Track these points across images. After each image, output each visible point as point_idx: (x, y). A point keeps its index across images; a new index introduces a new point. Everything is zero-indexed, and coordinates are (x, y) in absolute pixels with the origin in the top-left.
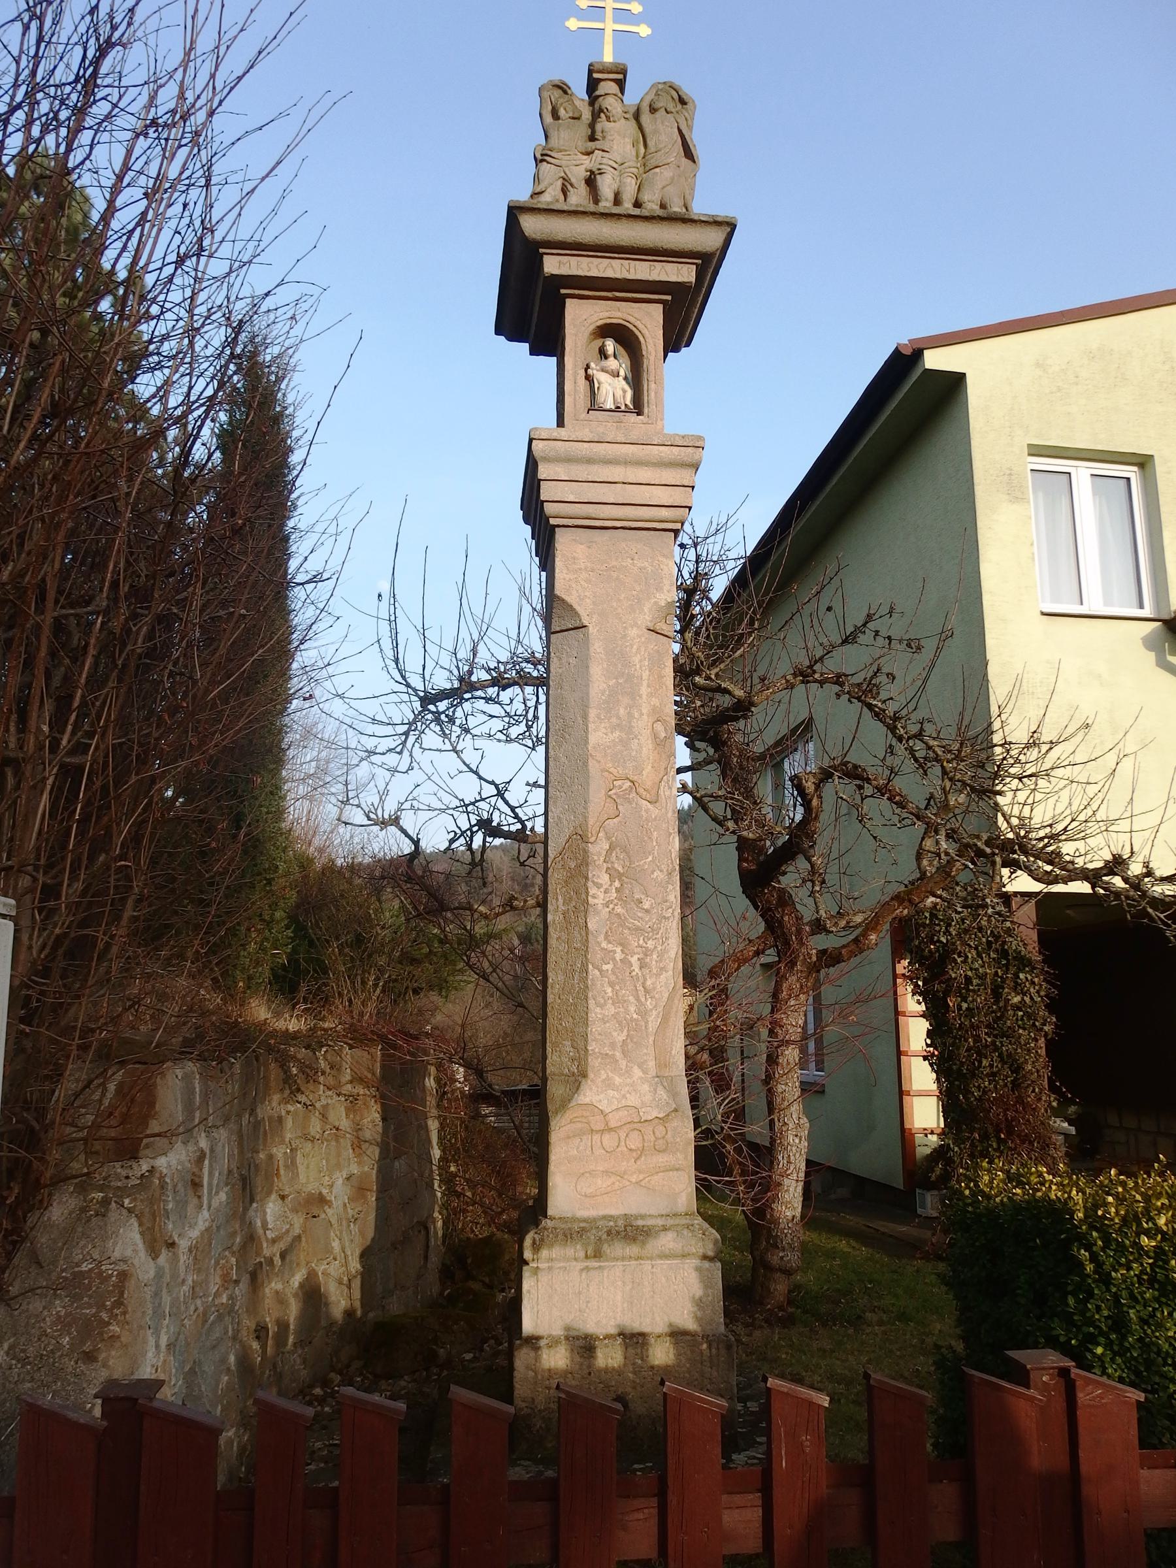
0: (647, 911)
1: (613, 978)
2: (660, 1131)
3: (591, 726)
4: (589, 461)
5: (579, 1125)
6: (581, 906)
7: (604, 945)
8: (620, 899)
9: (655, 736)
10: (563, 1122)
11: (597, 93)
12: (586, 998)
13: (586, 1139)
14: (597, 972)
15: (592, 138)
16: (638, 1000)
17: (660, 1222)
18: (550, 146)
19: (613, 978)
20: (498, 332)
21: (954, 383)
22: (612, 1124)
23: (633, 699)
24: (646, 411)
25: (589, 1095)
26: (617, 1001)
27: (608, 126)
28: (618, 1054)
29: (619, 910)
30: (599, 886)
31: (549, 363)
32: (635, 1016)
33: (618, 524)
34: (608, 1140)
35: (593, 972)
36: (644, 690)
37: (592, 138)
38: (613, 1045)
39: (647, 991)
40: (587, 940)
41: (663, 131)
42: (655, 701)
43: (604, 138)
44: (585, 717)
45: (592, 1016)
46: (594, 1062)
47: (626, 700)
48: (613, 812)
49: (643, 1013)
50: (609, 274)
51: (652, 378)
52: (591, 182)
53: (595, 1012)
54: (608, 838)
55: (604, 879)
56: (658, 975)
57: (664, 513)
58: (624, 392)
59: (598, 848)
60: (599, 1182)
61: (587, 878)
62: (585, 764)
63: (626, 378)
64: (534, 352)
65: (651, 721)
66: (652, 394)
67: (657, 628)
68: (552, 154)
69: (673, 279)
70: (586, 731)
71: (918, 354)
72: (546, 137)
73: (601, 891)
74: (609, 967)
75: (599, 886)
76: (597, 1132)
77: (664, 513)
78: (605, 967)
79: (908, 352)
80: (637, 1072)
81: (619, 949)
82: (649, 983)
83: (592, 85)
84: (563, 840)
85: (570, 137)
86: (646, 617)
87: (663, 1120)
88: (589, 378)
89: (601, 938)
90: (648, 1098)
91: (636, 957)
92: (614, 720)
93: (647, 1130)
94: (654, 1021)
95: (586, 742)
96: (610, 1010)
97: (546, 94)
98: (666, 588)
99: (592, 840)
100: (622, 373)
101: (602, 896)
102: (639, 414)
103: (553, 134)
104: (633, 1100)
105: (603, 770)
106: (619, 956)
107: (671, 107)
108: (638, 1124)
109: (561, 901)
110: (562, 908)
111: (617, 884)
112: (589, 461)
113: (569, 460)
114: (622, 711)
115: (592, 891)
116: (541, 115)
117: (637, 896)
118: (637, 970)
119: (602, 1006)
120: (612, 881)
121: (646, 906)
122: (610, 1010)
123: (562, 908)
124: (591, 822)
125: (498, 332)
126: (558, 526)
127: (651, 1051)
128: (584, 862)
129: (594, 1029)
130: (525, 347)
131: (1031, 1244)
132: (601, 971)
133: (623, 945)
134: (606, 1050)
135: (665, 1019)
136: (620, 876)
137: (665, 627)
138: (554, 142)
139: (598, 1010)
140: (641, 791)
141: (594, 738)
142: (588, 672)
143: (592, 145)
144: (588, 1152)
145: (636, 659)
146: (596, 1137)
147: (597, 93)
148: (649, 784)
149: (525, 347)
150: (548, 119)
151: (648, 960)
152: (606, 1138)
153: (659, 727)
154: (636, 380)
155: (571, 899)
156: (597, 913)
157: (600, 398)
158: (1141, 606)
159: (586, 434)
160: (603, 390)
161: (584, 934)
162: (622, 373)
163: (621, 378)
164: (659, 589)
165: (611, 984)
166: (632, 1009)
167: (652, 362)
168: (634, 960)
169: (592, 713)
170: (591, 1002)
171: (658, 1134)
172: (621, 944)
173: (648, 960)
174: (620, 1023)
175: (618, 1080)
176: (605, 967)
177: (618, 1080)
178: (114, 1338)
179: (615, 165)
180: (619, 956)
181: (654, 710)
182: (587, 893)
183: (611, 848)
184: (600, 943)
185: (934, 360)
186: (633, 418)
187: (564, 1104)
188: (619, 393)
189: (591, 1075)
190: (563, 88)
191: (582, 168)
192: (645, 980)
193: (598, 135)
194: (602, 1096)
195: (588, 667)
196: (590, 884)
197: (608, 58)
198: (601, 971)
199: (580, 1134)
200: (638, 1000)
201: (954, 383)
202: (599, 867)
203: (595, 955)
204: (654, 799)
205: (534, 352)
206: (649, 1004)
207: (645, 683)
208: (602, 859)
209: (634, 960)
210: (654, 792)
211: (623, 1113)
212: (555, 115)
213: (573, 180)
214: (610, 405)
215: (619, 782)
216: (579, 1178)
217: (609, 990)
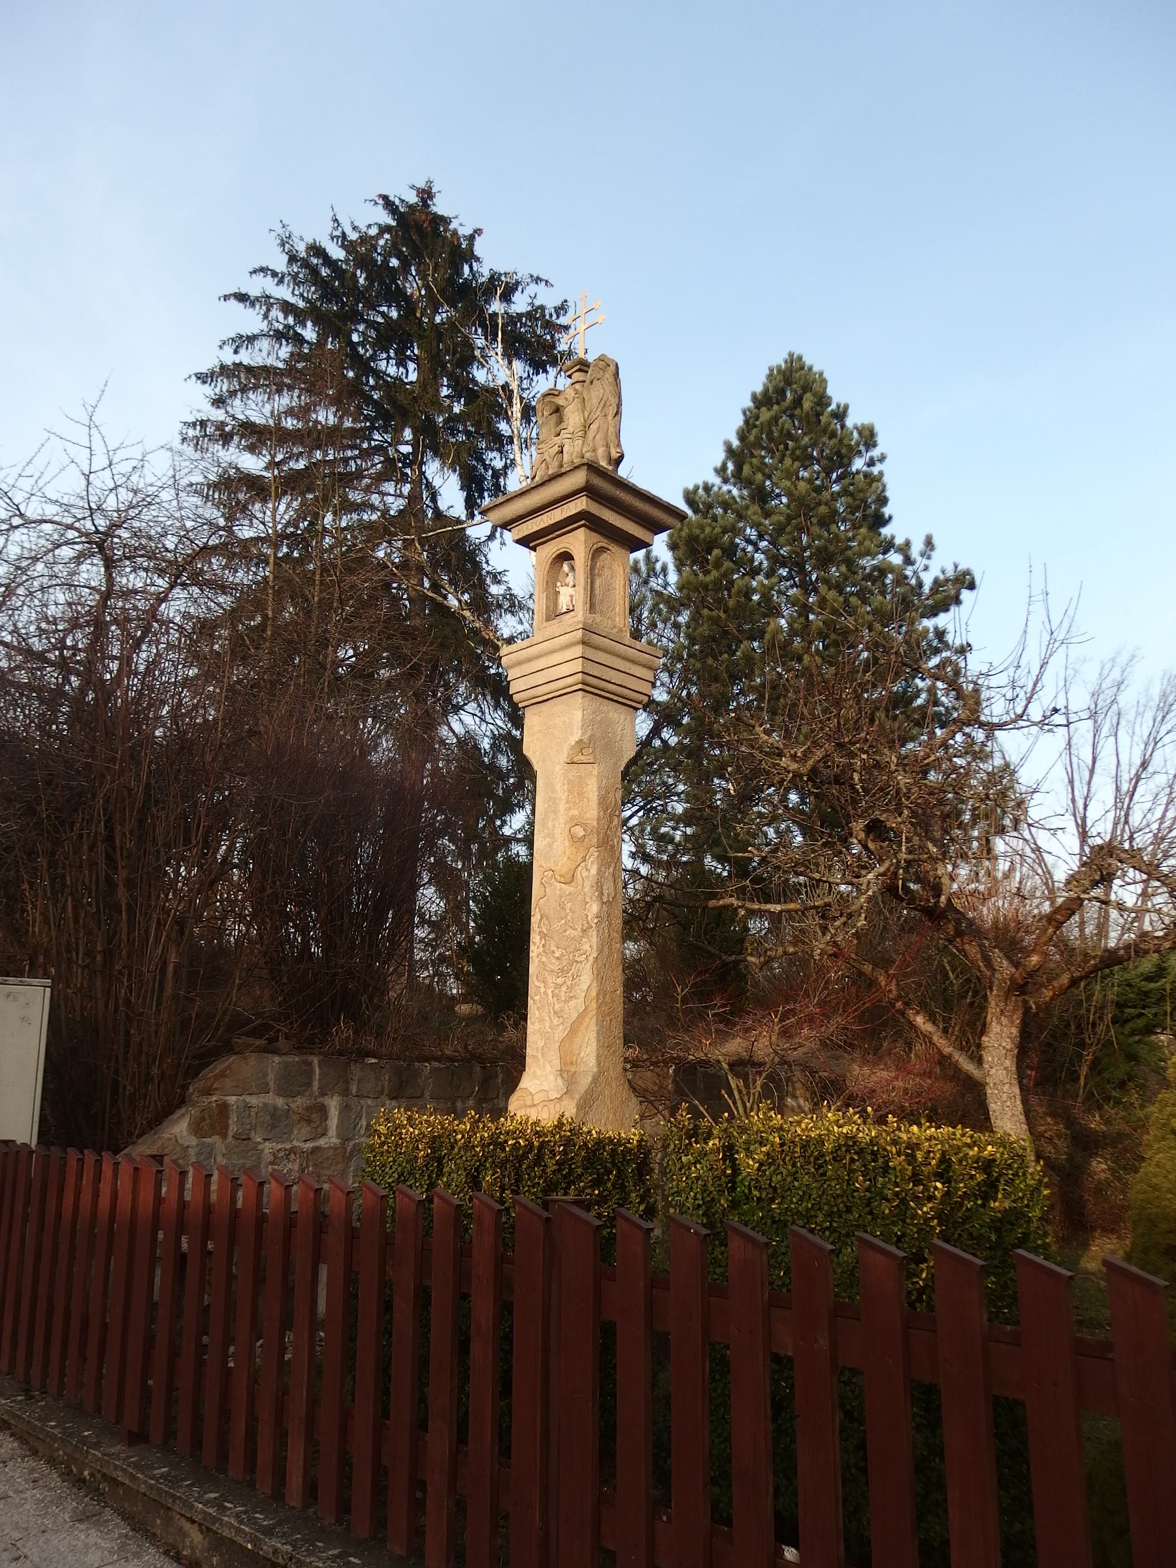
4: (529, 660)
29: (544, 959)
33: (550, 696)
47: (552, 816)
50: (542, 526)
57: (570, 680)
60: (1133, 936)
65: (568, 827)
67: (575, 760)
69: (574, 512)
77: (570, 680)
80: (548, 1068)
86: (564, 757)
87: (560, 1099)
90: (552, 1085)
93: (551, 1105)
104: (546, 1087)
112: (529, 660)
113: (519, 663)
137: (583, 758)
159: (547, 635)
164: (572, 734)
165: (538, 1009)
168: (549, 992)
178: (599, 1133)
209: (549, 992)
211: (541, 1095)
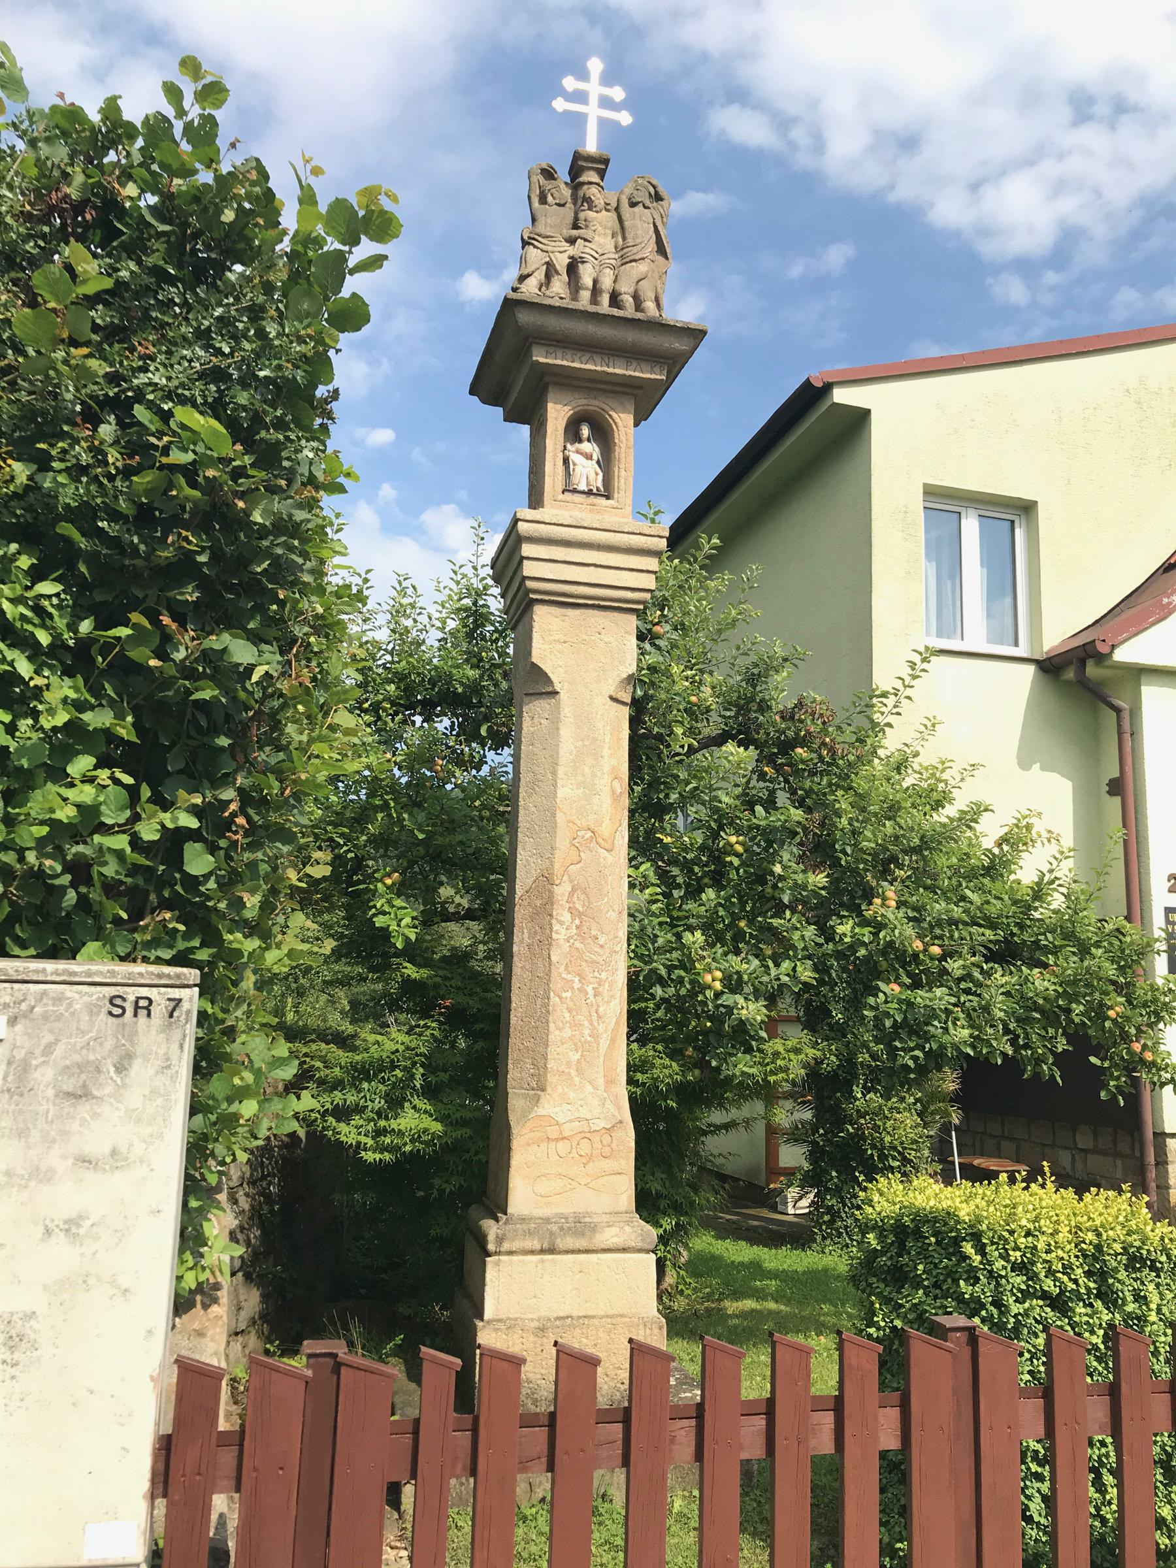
0: (602, 946)
1: (571, 1004)
2: (606, 1139)
3: (560, 783)
5: (539, 1134)
6: (545, 941)
7: (564, 976)
8: (579, 935)
9: (613, 791)
10: (524, 1131)
11: (581, 179)
12: (547, 1022)
13: (544, 1145)
14: (557, 999)
15: (576, 226)
16: (592, 1024)
17: (605, 1218)
18: (537, 231)
19: (571, 1004)
20: (472, 392)
21: (860, 418)
22: (566, 1134)
23: (596, 759)
24: (616, 495)
25: (548, 1107)
26: (575, 1025)
27: (591, 214)
28: (573, 1073)
29: (578, 945)
30: (561, 923)
31: (524, 431)
32: (589, 1039)
34: (562, 1147)
35: (554, 1000)
36: (606, 752)
37: (576, 226)
38: (569, 1064)
39: (599, 1017)
40: (550, 970)
41: (640, 223)
42: (614, 762)
43: (587, 226)
44: (554, 773)
45: (551, 1037)
46: (551, 1079)
48: (576, 859)
49: (595, 1036)
51: (622, 466)
52: (573, 268)
53: (555, 1035)
54: (571, 881)
55: (566, 917)
56: (608, 1002)
58: (597, 474)
59: (562, 890)
61: (551, 915)
62: (554, 815)
63: (598, 462)
64: (508, 418)
66: (622, 481)
68: (540, 239)
70: (555, 786)
71: (828, 388)
72: (534, 220)
73: (563, 927)
74: (568, 994)
75: (561, 923)
76: (553, 1140)
78: (564, 995)
79: (819, 384)
80: (589, 1088)
81: (576, 979)
82: (601, 1009)
83: (575, 171)
84: (530, 881)
85: (555, 219)
88: (566, 461)
89: (562, 969)
91: (591, 986)
92: (580, 778)
93: (596, 1139)
94: (604, 1044)
95: (555, 796)
96: (568, 1032)
97: (534, 179)
98: (629, 661)
99: (557, 882)
100: (595, 457)
101: (563, 931)
102: (608, 497)
103: (541, 220)
104: (584, 1113)
105: (569, 822)
106: (577, 985)
107: (648, 203)
108: (588, 1135)
109: (526, 935)
110: (527, 940)
111: (577, 922)
114: (587, 770)
115: (556, 927)
116: (529, 197)
117: (594, 933)
118: (592, 998)
119: (560, 1029)
120: (573, 919)
121: (602, 941)
122: (568, 1032)
123: (527, 940)
124: (557, 866)
125: (472, 392)
126: (537, 600)
127: (601, 1068)
128: (550, 901)
129: (552, 1051)
130: (499, 411)
131: (927, 1241)
132: (560, 998)
133: (582, 977)
134: (563, 1068)
135: (613, 1041)
136: (580, 914)
138: (541, 228)
139: (557, 1032)
140: (601, 841)
141: (561, 793)
142: (558, 734)
143: (575, 233)
144: (545, 1158)
145: (600, 725)
146: (552, 1145)
147: (581, 179)
148: (606, 834)
149: (499, 411)
150: (536, 204)
151: (601, 989)
152: (560, 1145)
153: (616, 784)
154: (606, 463)
155: (536, 933)
156: (559, 946)
157: (575, 480)
158: (1016, 644)
159: (565, 516)
160: (578, 469)
161: (547, 964)
162: (595, 457)
163: (594, 462)
166: (587, 1032)
167: (623, 450)
168: (590, 989)
169: (561, 771)
170: (551, 1025)
171: (605, 1143)
172: (579, 975)
173: (601, 989)
174: (575, 1044)
175: (572, 1095)
176: (564, 995)
177: (572, 1095)
179: (596, 256)
180: (577, 985)
181: (613, 769)
182: (551, 929)
183: (574, 890)
184: (560, 973)
185: (841, 396)
186: (602, 501)
187: (524, 1116)
188: (592, 476)
189: (549, 1090)
190: (548, 174)
191: (566, 255)
192: (598, 1006)
193: (582, 223)
194: (558, 1109)
195: (558, 729)
196: (554, 921)
197: (591, 147)
198: (560, 998)
199: (537, 1142)
200: (592, 1024)
201: (860, 418)
202: (562, 906)
203: (556, 984)
204: (610, 847)
205: (508, 418)
206: (601, 1028)
207: (607, 746)
208: (565, 899)
209: (590, 989)
210: (610, 841)
212: (543, 200)
213: (558, 267)
214: (583, 487)
215: (582, 833)
216: (537, 1178)
217: (567, 1015)
